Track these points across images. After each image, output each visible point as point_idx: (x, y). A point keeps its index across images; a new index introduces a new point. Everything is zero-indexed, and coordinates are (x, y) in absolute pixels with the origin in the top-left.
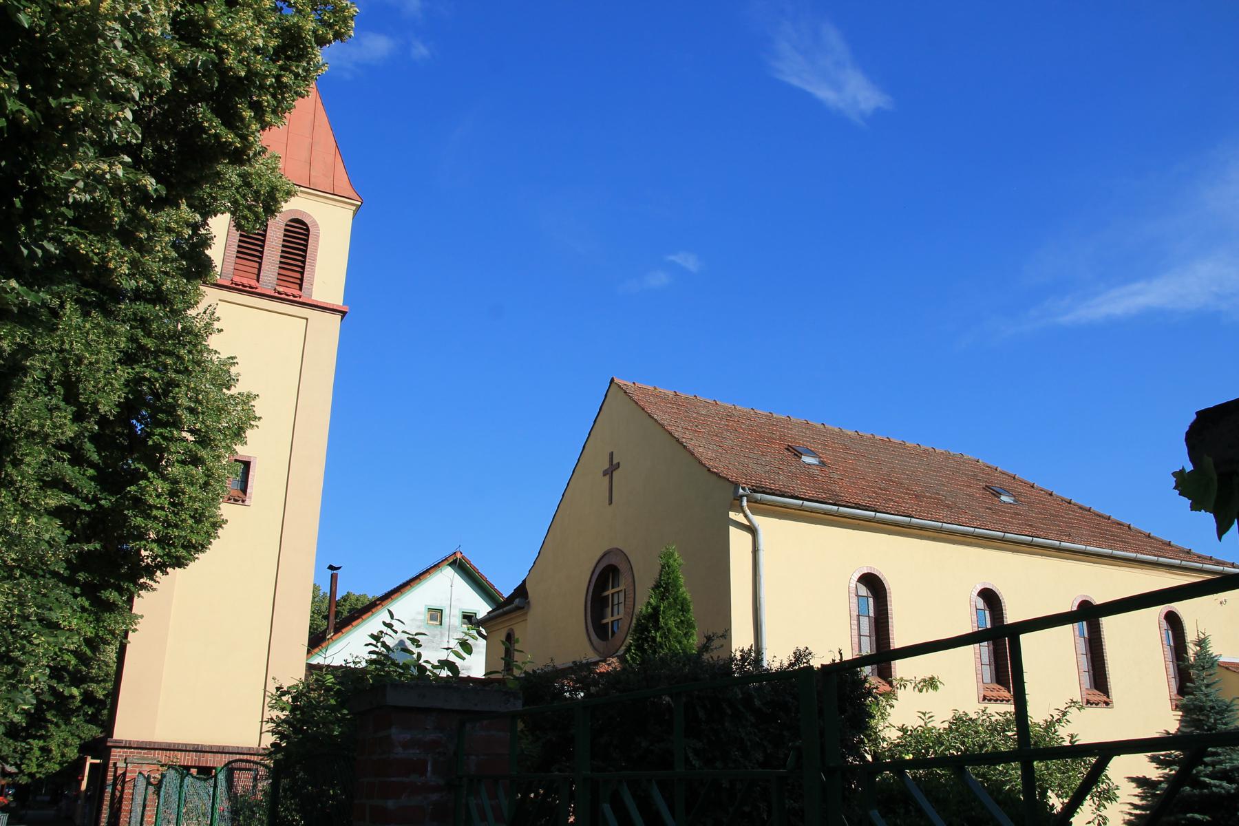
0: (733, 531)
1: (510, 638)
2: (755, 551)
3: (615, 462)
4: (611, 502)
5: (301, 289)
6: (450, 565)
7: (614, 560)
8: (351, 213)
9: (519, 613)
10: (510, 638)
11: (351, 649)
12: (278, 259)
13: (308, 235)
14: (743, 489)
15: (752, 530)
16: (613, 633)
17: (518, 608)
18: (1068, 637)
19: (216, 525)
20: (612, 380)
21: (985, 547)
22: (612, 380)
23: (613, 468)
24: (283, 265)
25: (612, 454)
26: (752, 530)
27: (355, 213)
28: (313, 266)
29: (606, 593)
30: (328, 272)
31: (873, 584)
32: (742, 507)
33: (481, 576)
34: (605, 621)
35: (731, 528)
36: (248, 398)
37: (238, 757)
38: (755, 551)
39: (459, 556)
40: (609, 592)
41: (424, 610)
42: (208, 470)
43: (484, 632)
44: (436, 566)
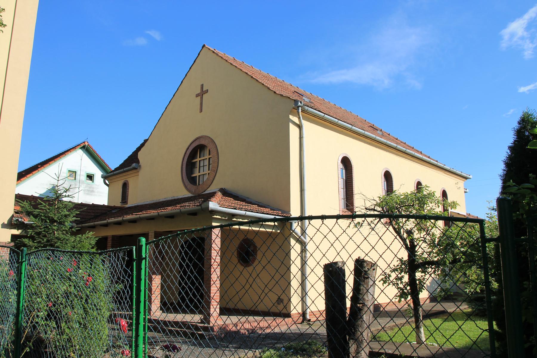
1: (125, 186)
2: (301, 138)
4: (201, 111)
6: (81, 148)
7: (203, 142)
9: (135, 171)
10: (125, 186)
11: (36, 186)
14: (301, 102)
15: (300, 127)
16: (199, 184)
17: (135, 169)
18: (359, 205)
20: (204, 46)
22: (204, 46)
23: (202, 93)
25: (202, 85)
26: (300, 127)
31: (346, 162)
32: (298, 112)
33: (98, 155)
34: (194, 175)
35: (291, 124)
38: (301, 138)
39: (87, 144)
40: (198, 159)
43: (107, 182)
44: (74, 148)
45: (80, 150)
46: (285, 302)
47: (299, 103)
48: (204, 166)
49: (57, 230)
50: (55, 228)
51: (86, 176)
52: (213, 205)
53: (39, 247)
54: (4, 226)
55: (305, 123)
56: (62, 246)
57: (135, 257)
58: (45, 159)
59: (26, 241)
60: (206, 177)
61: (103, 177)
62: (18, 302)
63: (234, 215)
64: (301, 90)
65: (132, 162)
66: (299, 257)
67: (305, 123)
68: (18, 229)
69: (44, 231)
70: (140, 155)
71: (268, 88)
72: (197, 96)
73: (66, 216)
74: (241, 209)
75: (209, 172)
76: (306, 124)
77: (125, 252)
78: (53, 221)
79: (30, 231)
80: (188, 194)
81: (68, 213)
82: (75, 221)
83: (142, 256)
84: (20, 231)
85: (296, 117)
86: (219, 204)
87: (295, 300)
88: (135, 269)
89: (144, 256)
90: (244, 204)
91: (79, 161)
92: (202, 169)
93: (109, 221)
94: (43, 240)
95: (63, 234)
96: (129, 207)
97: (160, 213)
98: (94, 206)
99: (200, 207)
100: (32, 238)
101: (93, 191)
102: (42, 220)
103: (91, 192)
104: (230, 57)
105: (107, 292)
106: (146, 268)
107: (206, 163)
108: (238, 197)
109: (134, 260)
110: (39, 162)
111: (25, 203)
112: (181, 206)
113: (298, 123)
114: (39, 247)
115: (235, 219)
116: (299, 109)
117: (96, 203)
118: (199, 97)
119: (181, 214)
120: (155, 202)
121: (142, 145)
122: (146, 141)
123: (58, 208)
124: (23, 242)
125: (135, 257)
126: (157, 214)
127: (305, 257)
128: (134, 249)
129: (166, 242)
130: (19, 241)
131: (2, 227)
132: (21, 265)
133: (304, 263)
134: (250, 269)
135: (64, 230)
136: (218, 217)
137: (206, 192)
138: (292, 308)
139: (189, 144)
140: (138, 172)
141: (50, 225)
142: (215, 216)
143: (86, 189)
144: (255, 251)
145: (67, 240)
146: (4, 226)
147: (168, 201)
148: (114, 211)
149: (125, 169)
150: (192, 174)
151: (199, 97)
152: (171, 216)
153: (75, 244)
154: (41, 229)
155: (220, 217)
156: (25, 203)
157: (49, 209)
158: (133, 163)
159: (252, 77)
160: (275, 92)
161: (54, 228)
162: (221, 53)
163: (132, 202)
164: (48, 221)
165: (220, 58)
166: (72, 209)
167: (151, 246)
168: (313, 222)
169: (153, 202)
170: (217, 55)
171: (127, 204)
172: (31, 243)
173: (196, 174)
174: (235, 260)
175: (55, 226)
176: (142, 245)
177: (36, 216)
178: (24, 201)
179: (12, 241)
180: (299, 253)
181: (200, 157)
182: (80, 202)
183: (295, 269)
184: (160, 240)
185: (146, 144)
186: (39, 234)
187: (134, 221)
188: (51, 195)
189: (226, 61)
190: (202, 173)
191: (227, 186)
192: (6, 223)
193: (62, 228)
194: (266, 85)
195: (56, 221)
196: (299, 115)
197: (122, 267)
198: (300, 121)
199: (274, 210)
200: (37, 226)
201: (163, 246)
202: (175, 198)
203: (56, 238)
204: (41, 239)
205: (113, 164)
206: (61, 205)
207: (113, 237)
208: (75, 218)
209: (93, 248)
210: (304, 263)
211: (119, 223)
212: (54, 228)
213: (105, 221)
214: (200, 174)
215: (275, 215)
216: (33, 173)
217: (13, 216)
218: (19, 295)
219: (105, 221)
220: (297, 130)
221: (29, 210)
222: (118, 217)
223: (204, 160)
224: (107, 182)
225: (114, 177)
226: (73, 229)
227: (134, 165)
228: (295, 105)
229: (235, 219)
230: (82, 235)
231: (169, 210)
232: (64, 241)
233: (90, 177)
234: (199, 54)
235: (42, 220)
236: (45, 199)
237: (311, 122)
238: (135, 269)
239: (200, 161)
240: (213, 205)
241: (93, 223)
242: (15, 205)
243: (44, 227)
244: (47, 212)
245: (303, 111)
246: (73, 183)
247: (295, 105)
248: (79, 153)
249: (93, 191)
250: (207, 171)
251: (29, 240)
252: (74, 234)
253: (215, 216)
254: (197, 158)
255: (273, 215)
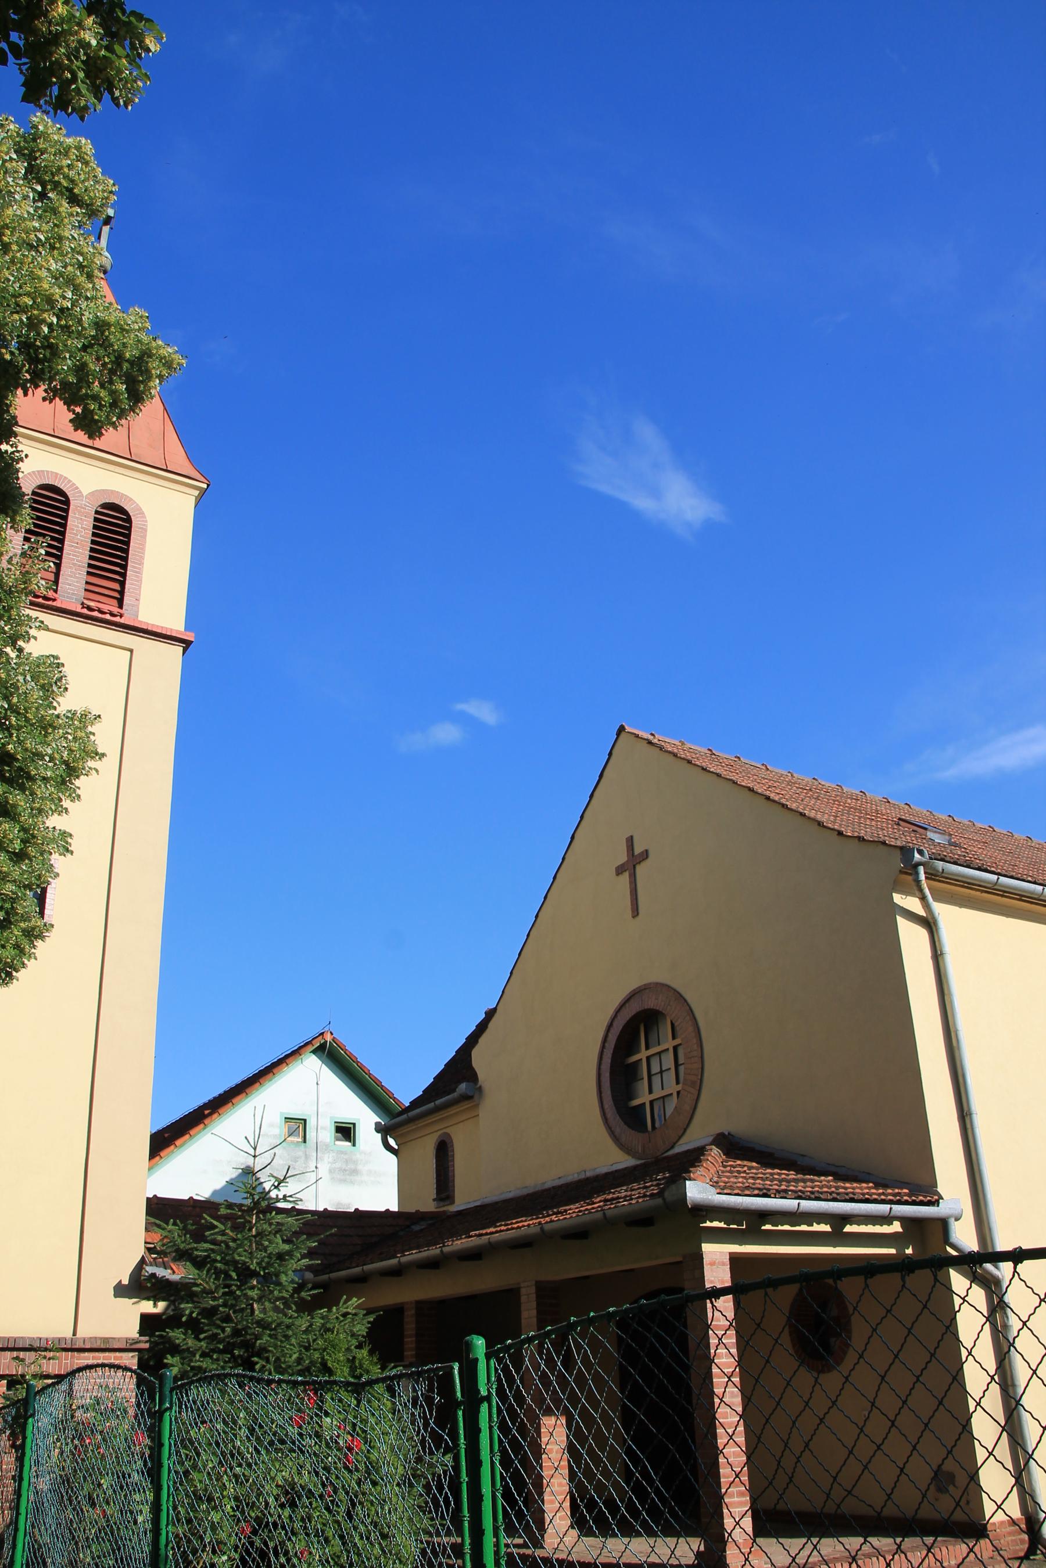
0: (902, 923)
1: (443, 1150)
2: (937, 956)
3: (638, 850)
4: (636, 912)
5: (121, 606)
6: (314, 1052)
7: (651, 1002)
8: (192, 501)
9: (466, 1105)
10: (443, 1150)
11: (199, 1171)
12: (87, 560)
13: (129, 529)
14: (921, 852)
15: (929, 923)
17: (466, 1097)
19: (34, 935)
20: (622, 729)
21: (956, 1031)
22: (622, 729)
23: (633, 861)
24: (93, 571)
25: (630, 841)
26: (929, 923)
27: (198, 501)
28: (139, 572)
29: (634, 1058)
30: (162, 578)
32: (918, 882)
34: (635, 1102)
35: (900, 921)
36: (84, 719)
37: (88, 1359)
38: (937, 956)
39: (328, 1038)
40: (642, 1055)
41: (279, 1121)
42: (24, 830)
43: (392, 1142)
44: (296, 1053)
45: (313, 1057)
46: (961, 1479)
47: (917, 855)
48: (661, 1072)
49: (260, 1300)
50: (254, 1294)
51: (333, 1129)
52: (697, 1190)
53: (213, 1351)
54: (120, 1291)
55: (943, 912)
56: (276, 1346)
57: (459, 1394)
58: (221, 1091)
59: (177, 1335)
60: (671, 1106)
61: (378, 1128)
62: (156, 1531)
63: (765, 1215)
64: (920, 812)
65: (457, 1081)
66: (995, 1388)
67: (943, 912)
68: (156, 1299)
69: (225, 1305)
70: (479, 1058)
71: (820, 824)
72: (620, 870)
73: (281, 1257)
74: (783, 1194)
75: (679, 1087)
76: (945, 913)
77: (431, 1381)
78: (245, 1274)
79: (187, 1307)
80: (625, 1161)
81: (287, 1247)
82: (309, 1268)
83: (478, 1391)
84: (162, 1305)
85: (913, 895)
86: (715, 1184)
87: (995, 1481)
88: (462, 1432)
89: (484, 1392)
90: (792, 1175)
91: (311, 1089)
92: (656, 1081)
93: (404, 1259)
94: (223, 1330)
95: (276, 1309)
96: (460, 1213)
97: (547, 1227)
98: (359, 1215)
99: (659, 1201)
100: (193, 1326)
101: (355, 1172)
102: (218, 1273)
103: (348, 1173)
104: (696, 749)
105: (406, 1482)
106: (491, 1428)
107: (668, 1061)
108: (770, 1155)
109: (458, 1404)
110: (206, 1099)
111: (170, 1227)
112: (606, 1201)
113: (922, 912)
114: (213, 1351)
115: (768, 1227)
116: (917, 874)
117: (364, 1207)
118: (626, 875)
119: (607, 1224)
120: (531, 1191)
121: (482, 1028)
122: (490, 1014)
123: (258, 1234)
124: (169, 1341)
125: (459, 1394)
126: (538, 1229)
127: (1006, 1326)
128: (456, 1372)
129: (541, 1346)
130: (161, 1336)
131: (116, 1296)
132: (161, 1420)
133: (1003, 1348)
134: (831, 1380)
135: (278, 1299)
136: (716, 1224)
137: (677, 1150)
138: (989, 1507)
139: (611, 1012)
140: (477, 1106)
141: (239, 1288)
142: (708, 1224)
143: (338, 1165)
144: (843, 1323)
145: (288, 1327)
146: (120, 1291)
147: (567, 1185)
148: (416, 1228)
149: (438, 1102)
150: (631, 1098)
151: (626, 875)
152: (579, 1234)
153: (311, 1337)
154: (214, 1299)
155: (722, 1225)
156: (170, 1227)
157: (234, 1240)
158: (460, 1082)
159: (768, 798)
160: (840, 833)
161: (250, 1293)
162: (671, 742)
163: (464, 1199)
164: (234, 1275)
165: (671, 757)
166: (296, 1234)
167: (500, 1361)
168: (1027, 1267)
169: (525, 1192)
170: (661, 748)
171: (453, 1202)
172: (191, 1342)
173: (643, 1098)
174: (785, 1358)
175: (253, 1288)
176: (477, 1360)
177: (199, 1264)
178: (167, 1224)
179: (141, 1332)
180: (992, 1372)
181: (647, 1048)
182: (321, 1209)
183: (977, 1376)
184: (523, 1342)
185: (491, 1025)
186: (210, 1313)
187: (473, 1256)
188: (237, 1199)
189: (689, 762)
190: (658, 1093)
191: (739, 1126)
192: (126, 1282)
193: (272, 1292)
194: (812, 814)
195: (254, 1274)
196: (921, 890)
197: (426, 1425)
198: (926, 906)
199: (885, 1186)
200: (204, 1291)
201: (532, 1358)
202: (589, 1174)
203: (260, 1323)
204: (218, 1327)
205: (406, 1090)
206: (266, 1226)
207: (421, 1306)
208: (305, 1261)
209: (359, 1346)
210: (1003, 1348)
211: (432, 1264)
212: (250, 1293)
213: (393, 1262)
214: (653, 1097)
215: (891, 1202)
216: (178, 1142)
217: (143, 1261)
218: (156, 1508)
219: (393, 1262)
220: (923, 933)
221: (182, 1246)
222: (429, 1244)
223: (659, 1053)
224: (392, 1142)
225: (412, 1127)
226: (303, 1294)
227: (463, 1087)
228: (905, 861)
229: (768, 1227)
230: (330, 1310)
231: (573, 1213)
232: (280, 1332)
233: (346, 1132)
234: (610, 754)
235: (218, 1273)
236: (223, 1211)
237: (961, 906)
238: (462, 1432)
239: (648, 1058)
240: (697, 1190)
241: (358, 1270)
242: (147, 1230)
243: (224, 1294)
244: (228, 1246)
245: (930, 876)
246: (300, 1151)
247: (905, 861)
248: (311, 1065)
249: (355, 1172)
250: (671, 1087)
251: (185, 1334)
252: (307, 1307)
253: (708, 1224)
254: (638, 1051)
255: (883, 1202)
